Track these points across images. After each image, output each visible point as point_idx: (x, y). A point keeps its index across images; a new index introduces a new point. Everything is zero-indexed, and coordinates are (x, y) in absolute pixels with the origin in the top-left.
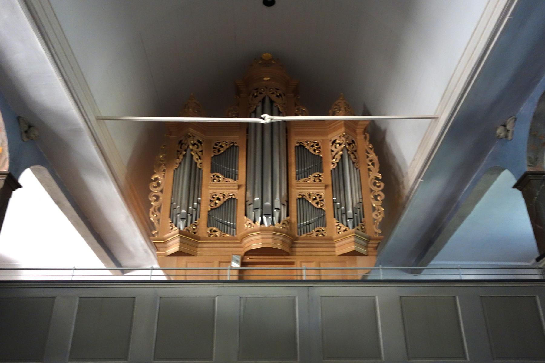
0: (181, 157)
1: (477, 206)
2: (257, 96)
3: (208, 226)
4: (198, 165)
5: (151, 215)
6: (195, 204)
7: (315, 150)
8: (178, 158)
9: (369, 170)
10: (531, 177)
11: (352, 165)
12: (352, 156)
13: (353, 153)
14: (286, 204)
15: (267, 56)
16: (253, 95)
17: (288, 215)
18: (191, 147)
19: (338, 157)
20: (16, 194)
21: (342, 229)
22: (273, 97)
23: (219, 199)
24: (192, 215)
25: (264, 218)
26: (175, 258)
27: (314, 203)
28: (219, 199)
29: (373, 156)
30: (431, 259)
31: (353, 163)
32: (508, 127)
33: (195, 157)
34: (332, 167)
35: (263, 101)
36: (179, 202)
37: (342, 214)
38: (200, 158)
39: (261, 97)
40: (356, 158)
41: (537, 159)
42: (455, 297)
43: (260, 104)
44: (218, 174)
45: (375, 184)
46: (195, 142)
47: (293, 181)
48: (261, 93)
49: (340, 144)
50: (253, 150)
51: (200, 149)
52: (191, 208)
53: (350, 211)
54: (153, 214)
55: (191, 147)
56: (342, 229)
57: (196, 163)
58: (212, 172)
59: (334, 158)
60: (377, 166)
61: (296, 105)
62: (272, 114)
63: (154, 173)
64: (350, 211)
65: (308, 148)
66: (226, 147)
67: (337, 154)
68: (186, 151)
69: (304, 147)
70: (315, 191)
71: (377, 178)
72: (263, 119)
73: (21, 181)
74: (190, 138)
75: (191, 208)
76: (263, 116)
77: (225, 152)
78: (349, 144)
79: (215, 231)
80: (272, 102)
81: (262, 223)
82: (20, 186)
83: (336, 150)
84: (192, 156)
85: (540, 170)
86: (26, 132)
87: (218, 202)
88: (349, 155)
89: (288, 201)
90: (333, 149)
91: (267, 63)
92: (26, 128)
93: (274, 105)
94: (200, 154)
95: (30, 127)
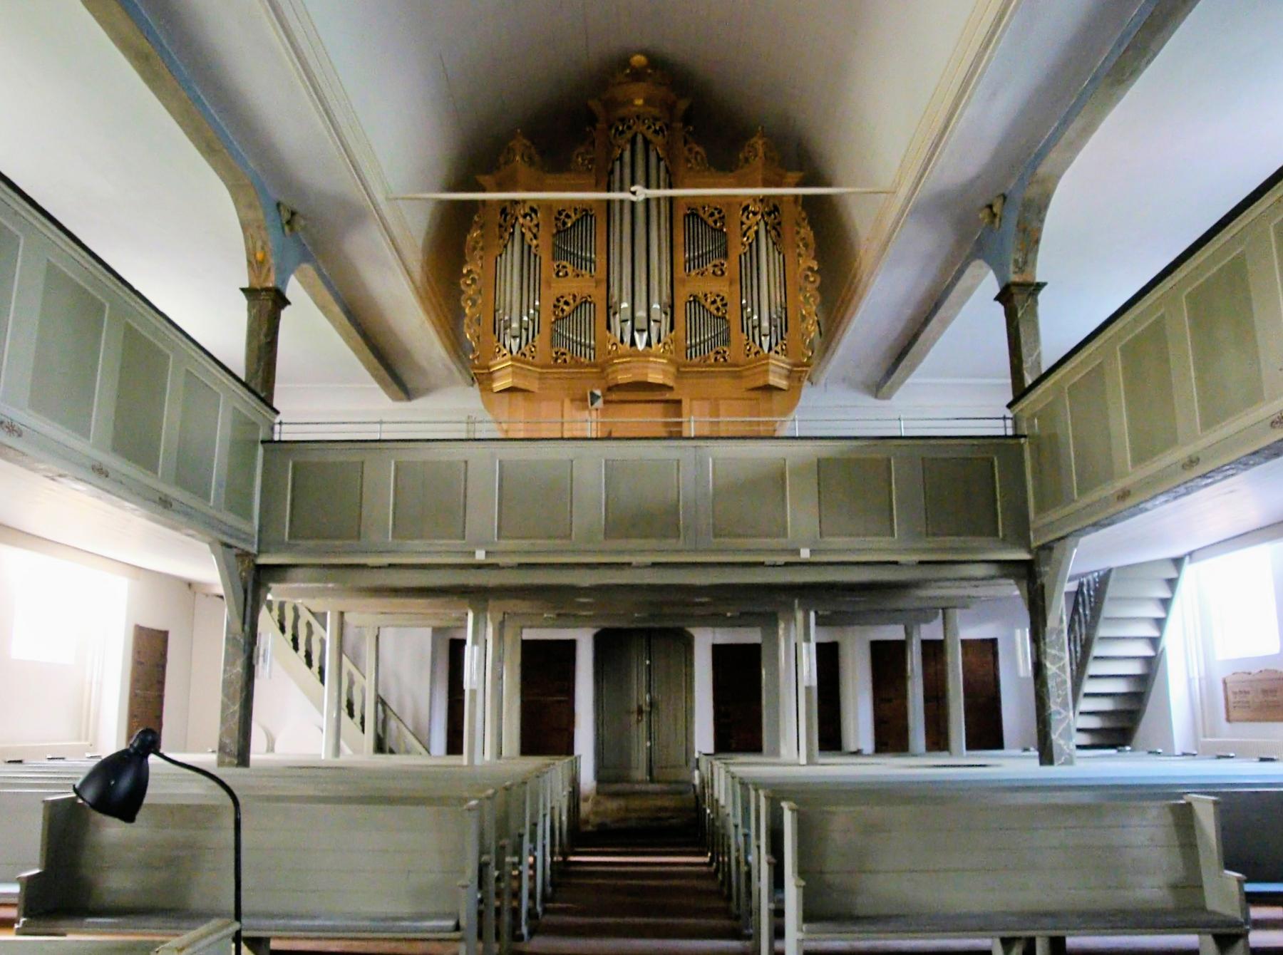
0: (507, 236)
1: (964, 308)
2: (623, 132)
3: (552, 346)
4: (533, 249)
5: (465, 329)
6: (532, 311)
7: (715, 222)
8: (501, 237)
9: (800, 255)
10: (1014, 290)
11: (771, 244)
12: (773, 233)
13: (774, 228)
14: (669, 311)
15: (639, 60)
16: (617, 129)
17: (672, 328)
18: (521, 220)
19: (751, 233)
20: (285, 314)
21: (753, 350)
22: (650, 134)
23: (567, 303)
24: (527, 329)
25: (636, 335)
26: (506, 395)
27: (713, 308)
28: (567, 303)
29: (806, 232)
30: (907, 376)
31: (774, 244)
32: (995, 210)
33: (529, 235)
34: (741, 250)
35: (633, 142)
36: (507, 310)
37: (754, 328)
38: (535, 237)
39: (629, 135)
40: (779, 235)
41: (1025, 263)
42: (889, 460)
43: (628, 147)
44: (565, 263)
45: (807, 277)
46: (527, 210)
47: (680, 272)
48: (629, 128)
49: (755, 214)
50: (617, 222)
51: (535, 222)
52: (525, 318)
53: (765, 324)
54: (469, 327)
55: (521, 220)
56: (753, 350)
57: (530, 247)
58: (554, 259)
59: (744, 235)
60: (812, 245)
61: (686, 142)
62: (648, 186)
63: (465, 262)
64: (765, 324)
65: (705, 216)
66: (574, 218)
67: (750, 228)
68: (513, 226)
69: (698, 216)
70: (715, 289)
71: (811, 269)
72: (634, 193)
73: (289, 295)
74: (520, 206)
75: (525, 318)
76: (633, 189)
77: (573, 225)
78: (769, 214)
79: (563, 354)
80: (647, 143)
81: (633, 343)
82: (289, 303)
83: (748, 223)
84: (523, 234)
85: (1029, 279)
86: (288, 222)
87: (565, 307)
88: (767, 231)
89: (672, 307)
90: (744, 219)
91: (638, 75)
92: (287, 216)
93: (651, 147)
94: (535, 230)
95: (293, 214)
